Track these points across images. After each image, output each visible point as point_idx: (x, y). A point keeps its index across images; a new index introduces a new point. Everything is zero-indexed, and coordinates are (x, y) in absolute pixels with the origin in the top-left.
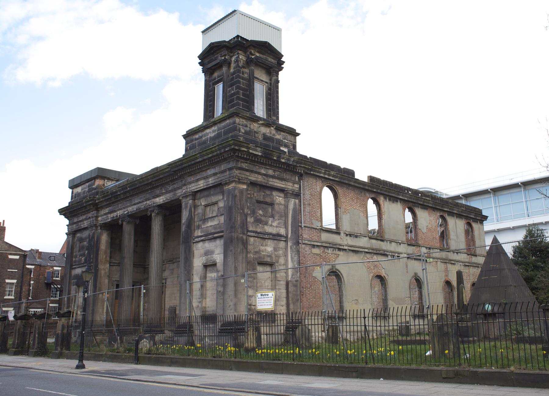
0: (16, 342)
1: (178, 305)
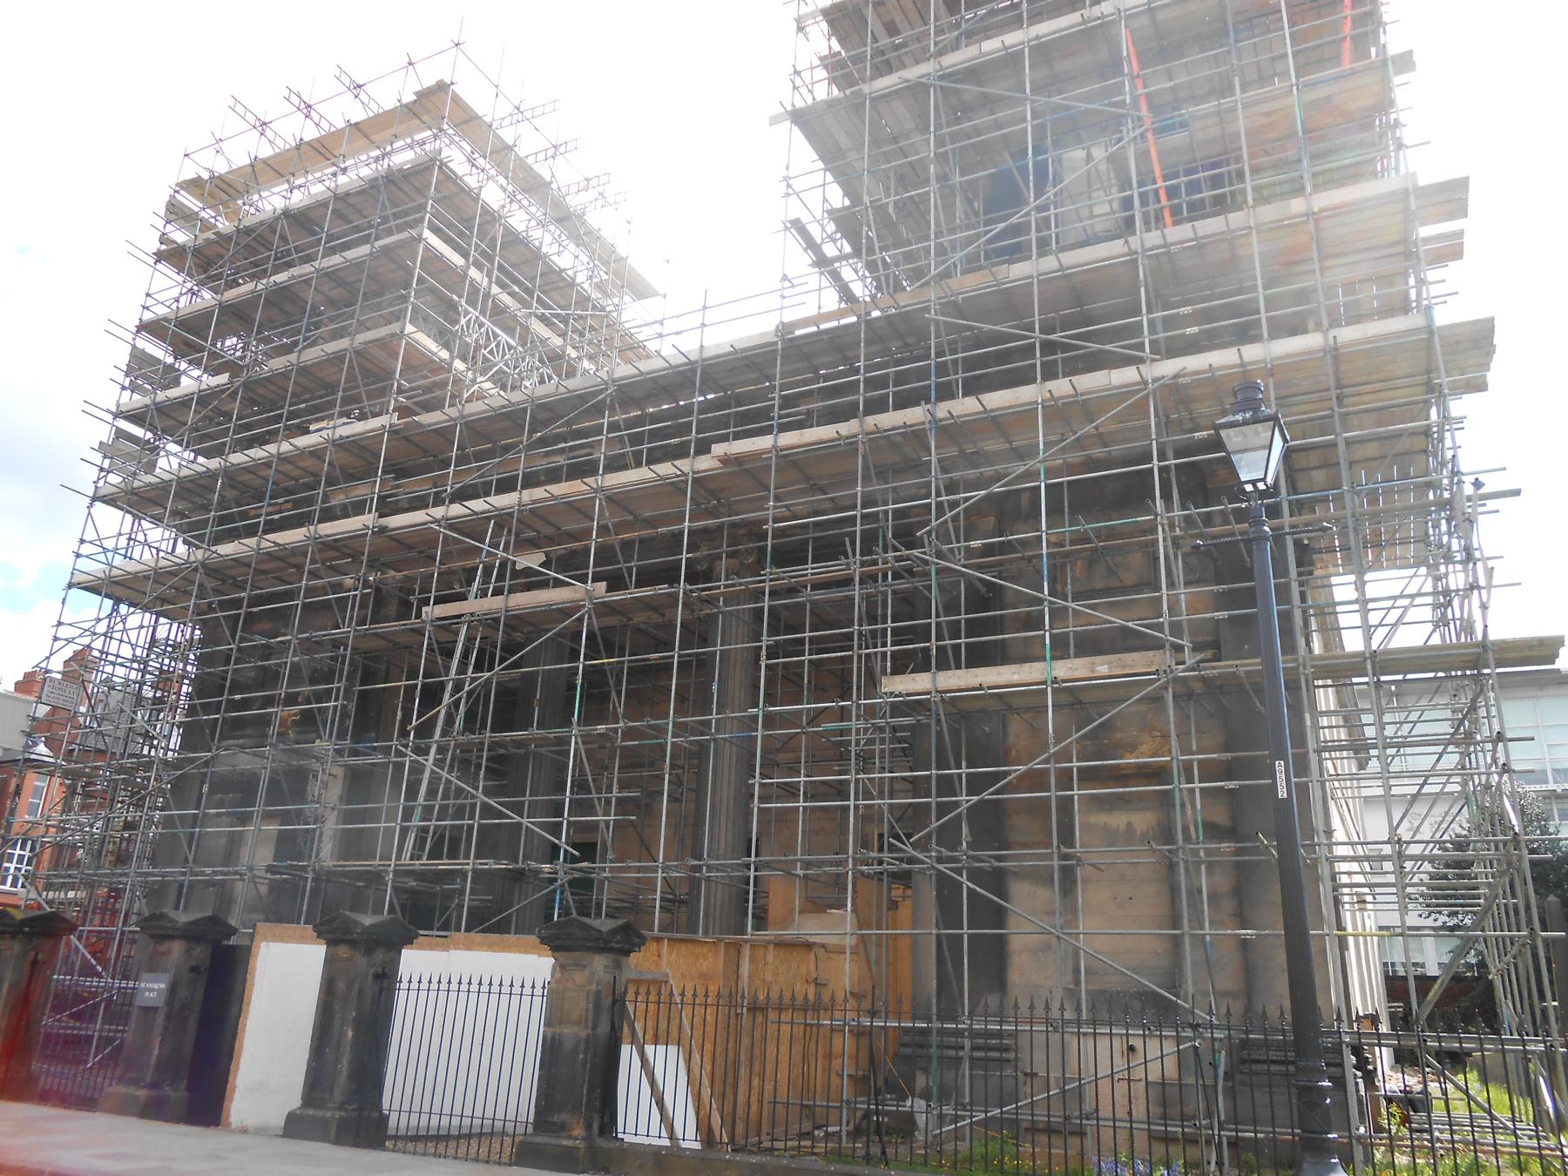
0: (156, 1052)
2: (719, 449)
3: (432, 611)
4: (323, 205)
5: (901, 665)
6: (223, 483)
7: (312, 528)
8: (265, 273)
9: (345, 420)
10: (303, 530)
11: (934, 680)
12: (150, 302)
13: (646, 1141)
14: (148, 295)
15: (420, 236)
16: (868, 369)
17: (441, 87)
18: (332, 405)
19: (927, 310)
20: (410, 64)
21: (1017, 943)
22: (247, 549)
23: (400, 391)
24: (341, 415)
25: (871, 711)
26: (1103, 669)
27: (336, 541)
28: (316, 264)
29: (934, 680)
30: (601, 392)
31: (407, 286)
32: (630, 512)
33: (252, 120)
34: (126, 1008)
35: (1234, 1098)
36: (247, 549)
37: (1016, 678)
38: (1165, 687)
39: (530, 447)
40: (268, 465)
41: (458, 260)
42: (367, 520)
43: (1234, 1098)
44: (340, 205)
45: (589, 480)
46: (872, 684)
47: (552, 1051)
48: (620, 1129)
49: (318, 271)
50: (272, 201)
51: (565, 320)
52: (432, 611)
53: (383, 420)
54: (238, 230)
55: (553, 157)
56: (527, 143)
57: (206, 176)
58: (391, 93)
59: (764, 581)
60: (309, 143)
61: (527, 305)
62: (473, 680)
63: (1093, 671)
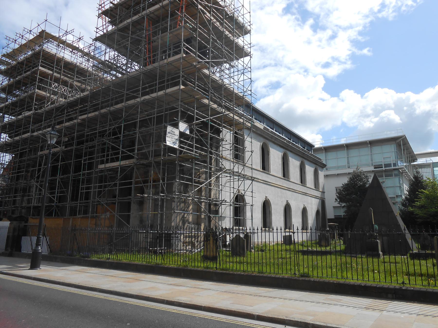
1: (43, 219)
2: (80, 118)
3: (40, 153)
4: (24, 60)
5: (102, 162)
6: (8, 126)
7: (99, 111)
8: (21, 74)
9: (27, 112)
10: (19, 137)
11: (105, 166)
12: (98, 30)
13: (25, 252)
14: (97, 28)
15: (38, 69)
16: (102, 100)
17: (43, 31)
18: (24, 109)
19: (110, 86)
20: (38, 25)
21: (132, 216)
22: (115, 109)
23: (35, 104)
24: (26, 111)
25: (96, 172)
26: (127, 163)
27: (26, 138)
28: (22, 75)
29: (105, 166)
30: (64, 105)
31: (36, 81)
32: (70, 132)
33: (11, 40)
34: (169, 238)
35: (243, 245)
36: (151, 97)
37: (116, 165)
38: (134, 166)
39: (55, 117)
40: (22, 119)
41: (50, 72)
42: (29, 134)
43: (243, 245)
44: (112, 13)
45: (61, 125)
46: (97, 167)
47: (8, 237)
48: (22, 250)
49: (23, 77)
50: (21, 58)
51: (85, 80)
52: (40, 153)
53: (31, 112)
54: (11, 67)
55: (79, 41)
56: (69, 39)
57: (6, 54)
58: (36, 32)
59: (95, 143)
60: (23, 45)
61: (73, 79)
62: (43, 168)
63: (126, 163)
